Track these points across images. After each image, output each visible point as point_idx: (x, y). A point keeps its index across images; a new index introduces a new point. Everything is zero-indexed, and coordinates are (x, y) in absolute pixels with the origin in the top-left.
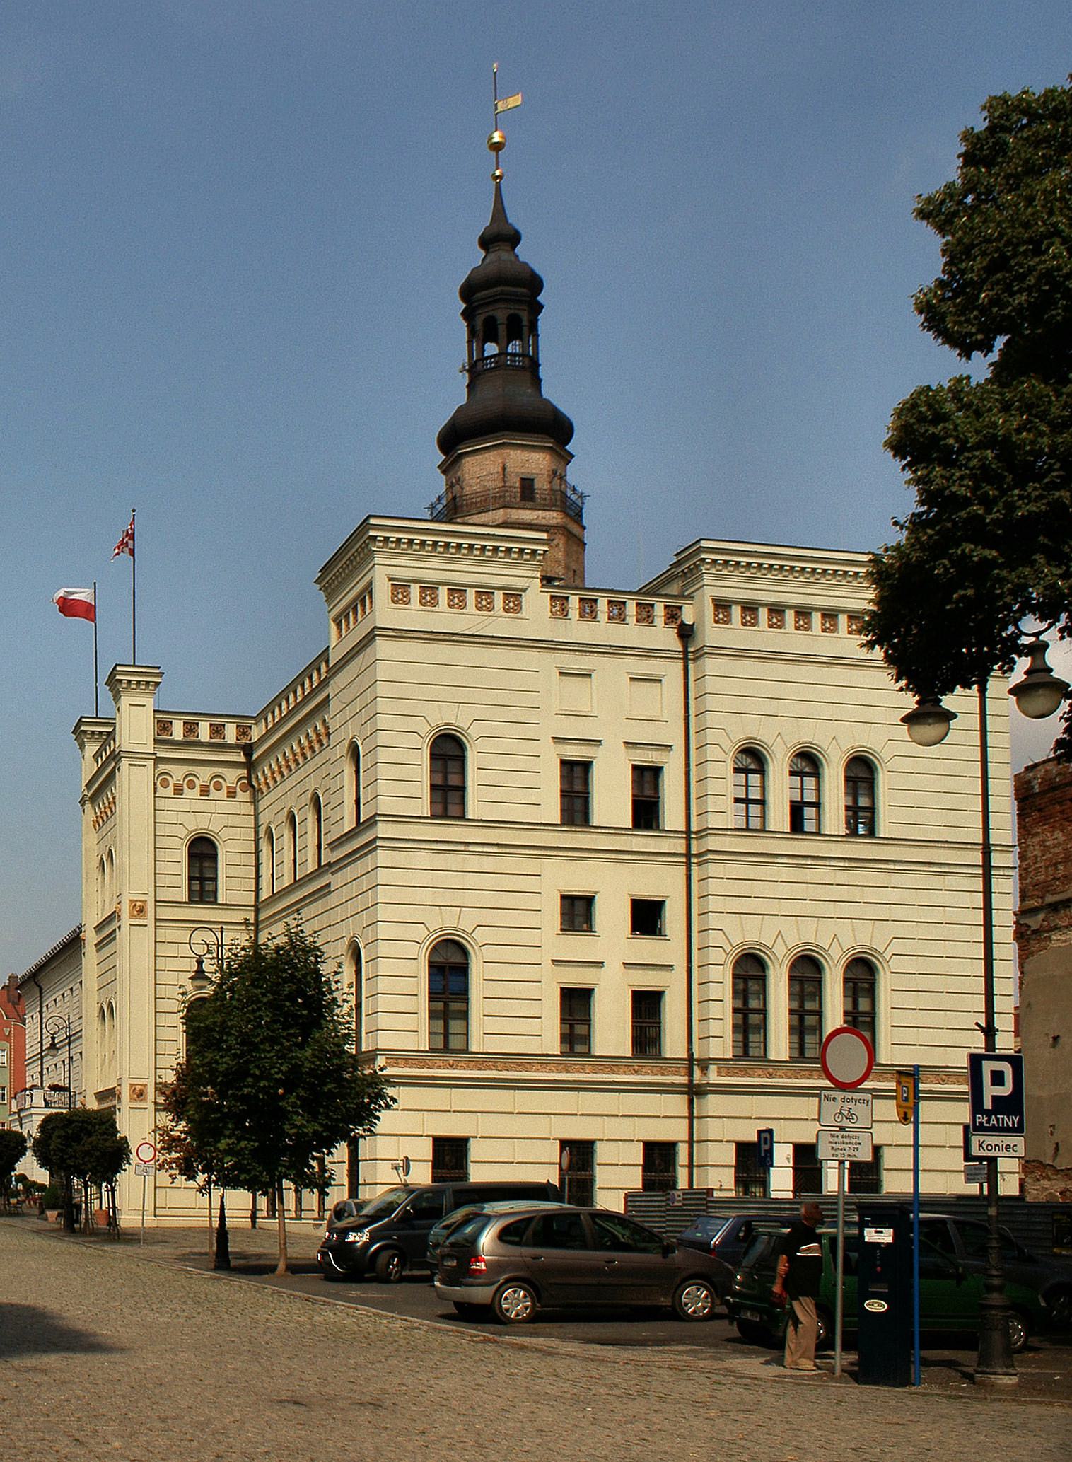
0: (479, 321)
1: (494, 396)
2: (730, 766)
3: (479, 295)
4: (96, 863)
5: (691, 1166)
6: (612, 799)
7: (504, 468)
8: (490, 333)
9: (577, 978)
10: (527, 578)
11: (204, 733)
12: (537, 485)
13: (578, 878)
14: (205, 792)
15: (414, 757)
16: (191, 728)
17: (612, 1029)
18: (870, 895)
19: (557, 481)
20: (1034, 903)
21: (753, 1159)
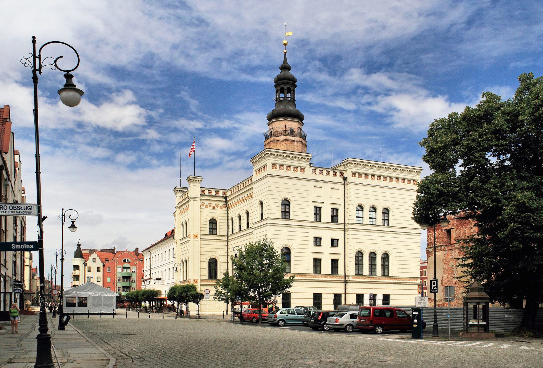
0: (279, 88)
1: (282, 108)
2: (355, 209)
5: (345, 299)
6: (326, 215)
8: (282, 91)
9: (318, 256)
10: (306, 164)
11: (214, 193)
13: (318, 233)
15: (277, 205)
16: (210, 192)
17: (326, 268)
18: (388, 239)
19: (299, 130)
20: (430, 246)
21: (360, 298)
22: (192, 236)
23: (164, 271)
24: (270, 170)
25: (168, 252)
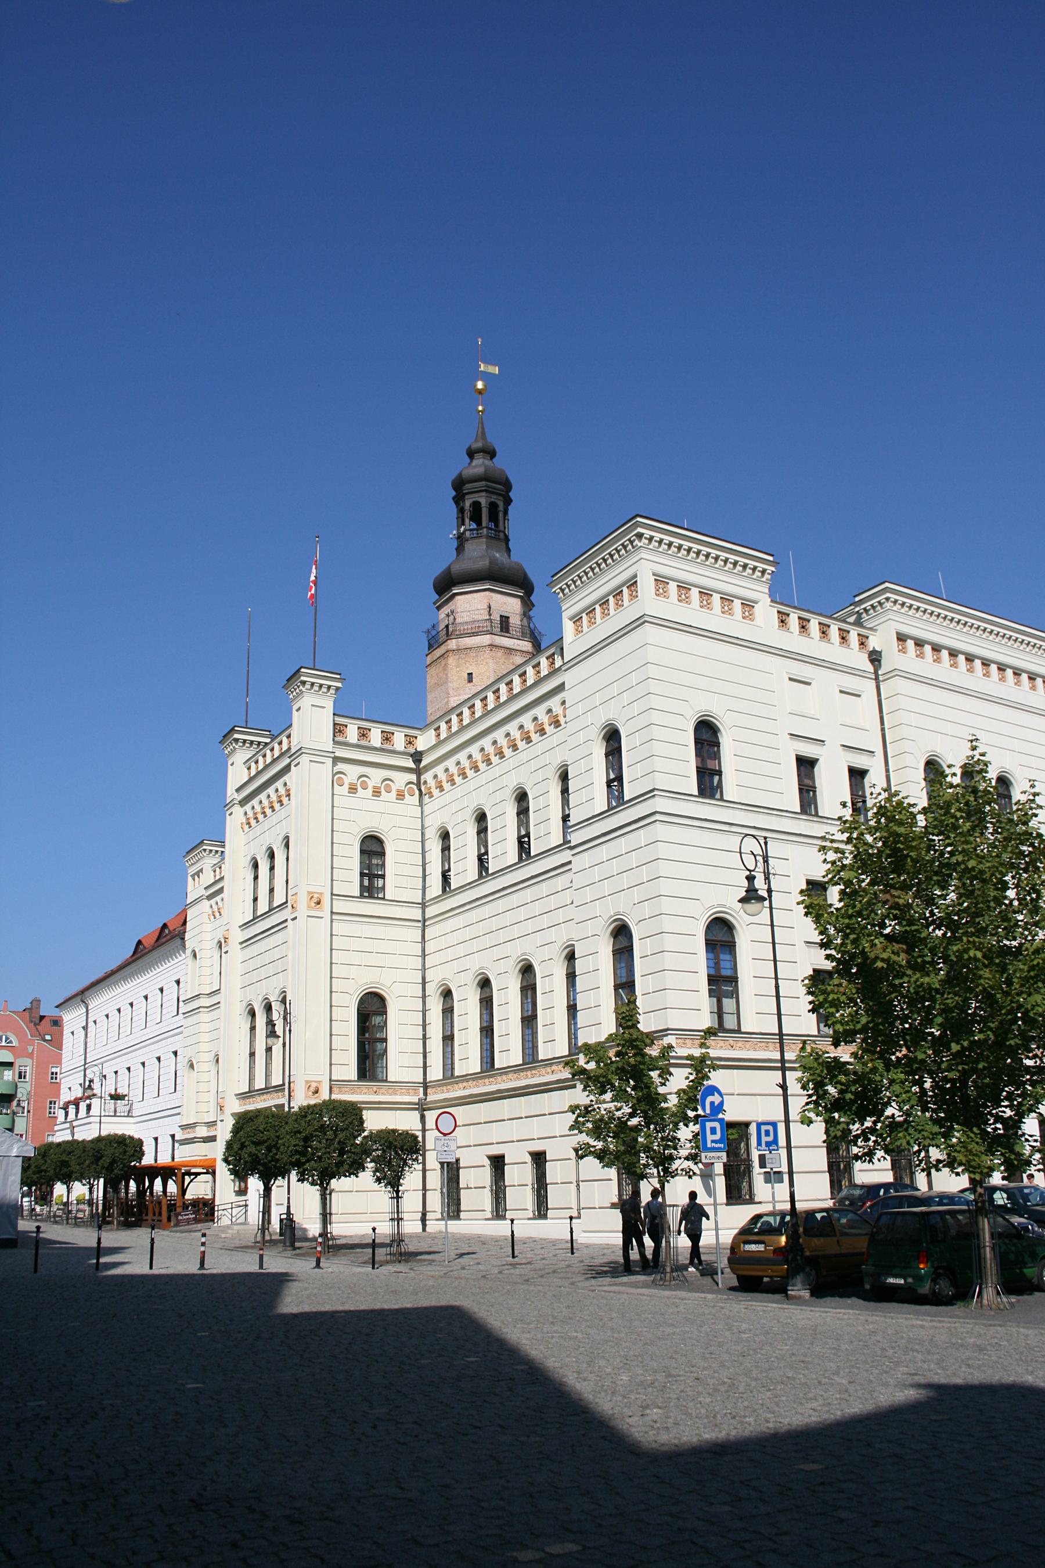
0: (467, 504)
1: (479, 554)
3: (468, 486)
4: (247, 862)
7: (490, 607)
10: (759, 591)
12: (511, 621)
14: (377, 793)
22: (302, 902)
23: (137, 1068)
24: (648, 600)
25: (155, 997)
